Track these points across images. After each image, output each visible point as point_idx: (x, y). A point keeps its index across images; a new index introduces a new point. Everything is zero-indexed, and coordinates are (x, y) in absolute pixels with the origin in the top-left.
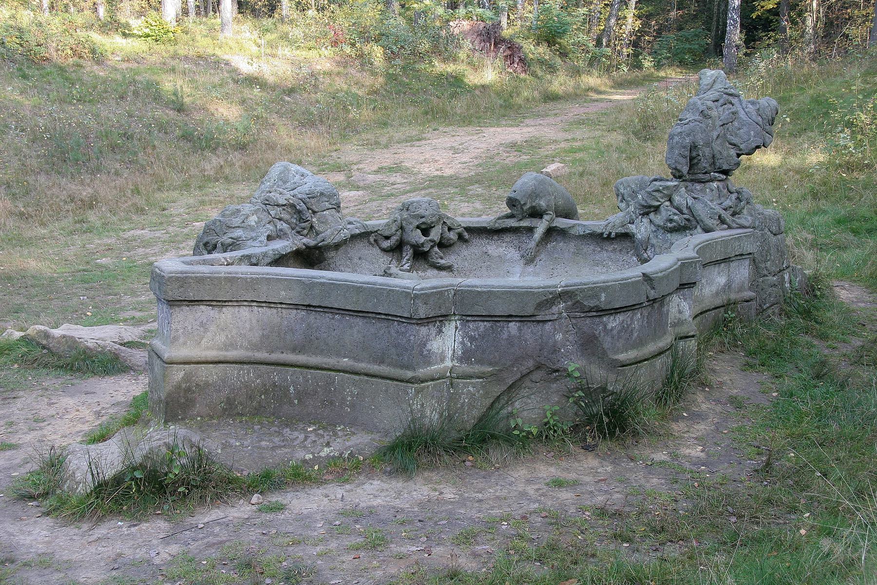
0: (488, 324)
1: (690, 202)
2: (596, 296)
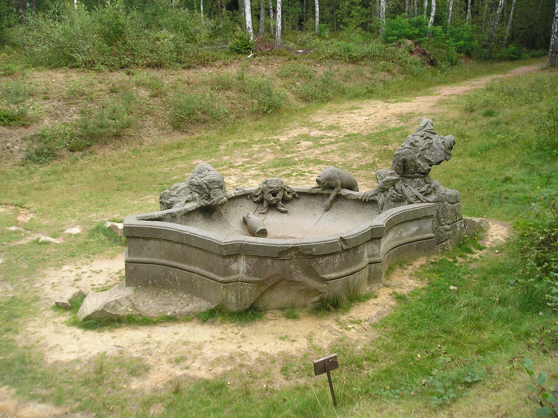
0: (257, 259)
2: (311, 250)
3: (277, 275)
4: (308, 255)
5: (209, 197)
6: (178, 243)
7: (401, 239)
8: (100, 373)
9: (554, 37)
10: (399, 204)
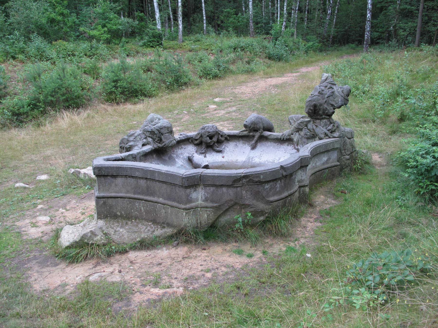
0: (214, 188)
1: (314, 127)
3: (231, 200)
4: (257, 182)
5: (160, 140)
6: (142, 178)
7: (316, 168)
8: (89, 298)
9: (367, 34)
10: (311, 141)
